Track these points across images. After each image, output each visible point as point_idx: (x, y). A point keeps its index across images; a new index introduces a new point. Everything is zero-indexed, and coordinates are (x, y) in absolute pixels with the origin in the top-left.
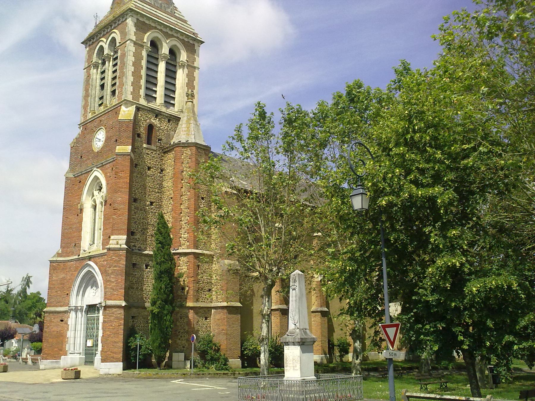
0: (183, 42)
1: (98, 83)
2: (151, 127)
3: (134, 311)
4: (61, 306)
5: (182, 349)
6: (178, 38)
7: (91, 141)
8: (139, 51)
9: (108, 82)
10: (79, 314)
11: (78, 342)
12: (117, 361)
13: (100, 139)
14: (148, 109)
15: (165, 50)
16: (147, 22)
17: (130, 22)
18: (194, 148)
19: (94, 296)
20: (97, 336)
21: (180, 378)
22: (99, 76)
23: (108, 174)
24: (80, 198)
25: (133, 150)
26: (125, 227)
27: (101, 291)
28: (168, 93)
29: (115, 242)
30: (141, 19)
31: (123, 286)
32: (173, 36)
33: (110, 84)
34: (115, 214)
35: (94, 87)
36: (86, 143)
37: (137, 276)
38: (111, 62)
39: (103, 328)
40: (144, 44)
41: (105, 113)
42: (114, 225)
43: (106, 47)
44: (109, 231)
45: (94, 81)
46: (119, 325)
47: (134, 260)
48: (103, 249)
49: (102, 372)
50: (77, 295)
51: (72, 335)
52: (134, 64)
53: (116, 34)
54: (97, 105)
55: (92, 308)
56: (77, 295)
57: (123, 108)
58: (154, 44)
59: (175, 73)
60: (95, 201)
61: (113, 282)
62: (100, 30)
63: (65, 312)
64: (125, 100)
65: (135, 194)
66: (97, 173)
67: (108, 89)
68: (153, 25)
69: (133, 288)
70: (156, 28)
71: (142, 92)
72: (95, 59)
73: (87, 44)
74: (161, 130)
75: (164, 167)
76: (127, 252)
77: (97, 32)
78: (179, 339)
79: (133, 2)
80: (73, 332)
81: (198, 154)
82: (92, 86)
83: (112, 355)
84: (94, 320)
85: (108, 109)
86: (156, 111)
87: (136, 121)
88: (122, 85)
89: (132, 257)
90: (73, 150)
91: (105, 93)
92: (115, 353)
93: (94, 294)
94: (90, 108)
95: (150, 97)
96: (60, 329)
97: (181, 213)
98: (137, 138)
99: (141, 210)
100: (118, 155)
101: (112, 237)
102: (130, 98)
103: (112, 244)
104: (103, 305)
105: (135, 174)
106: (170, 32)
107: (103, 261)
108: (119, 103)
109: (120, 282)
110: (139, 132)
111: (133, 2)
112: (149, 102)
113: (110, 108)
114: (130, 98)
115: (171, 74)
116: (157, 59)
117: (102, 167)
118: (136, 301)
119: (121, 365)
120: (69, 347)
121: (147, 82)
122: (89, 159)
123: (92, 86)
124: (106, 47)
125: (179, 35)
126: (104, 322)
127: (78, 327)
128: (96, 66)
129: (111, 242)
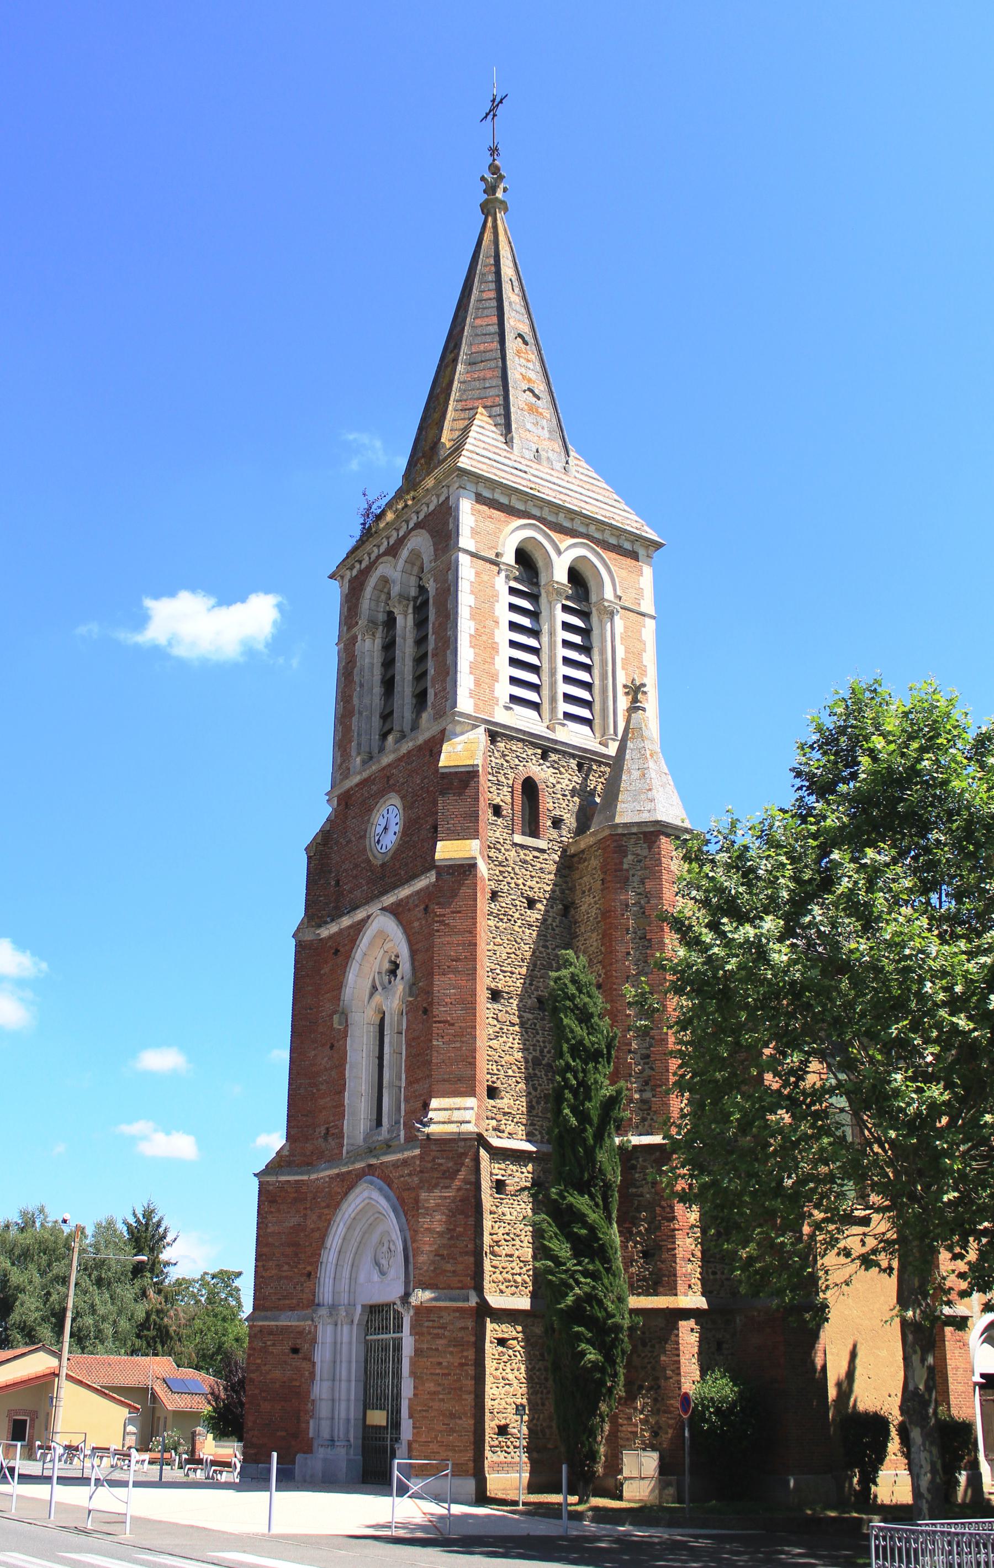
8: (485, 578)
20: (397, 1397)
33: (409, 676)
36: (349, 842)
37: (508, 1217)
38: (410, 618)
39: (413, 1373)
45: (367, 673)
46: (461, 1365)
80: (326, 1385)
82: (362, 686)
94: (359, 745)
101: (435, 1103)
107: (410, 1175)
110: (497, 801)
123: (362, 686)
126: (418, 1352)
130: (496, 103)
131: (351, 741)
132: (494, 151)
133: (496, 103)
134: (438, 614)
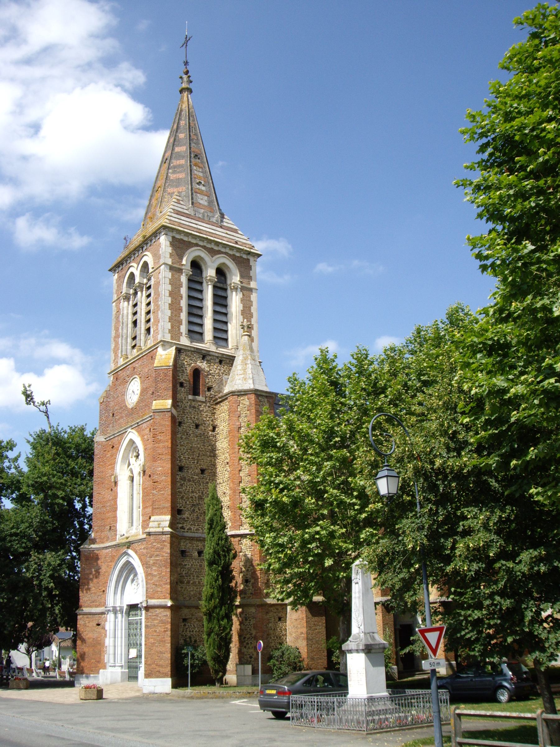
0: (234, 258)
1: (130, 319)
2: (197, 373)
3: (185, 612)
4: (97, 606)
5: (249, 659)
6: (226, 253)
7: (124, 394)
9: (142, 317)
10: (119, 616)
11: (119, 652)
12: (164, 676)
13: (134, 391)
14: (193, 349)
15: (210, 273)
16: (186, 239)
17: (164, 240)
18: (253, 397)
19: (135, 593)
20: (141, 645)
21: (244, 698)
22: (130, 311)
23: (146, 437)
24: (113, 468)
25: (175, 404)
26: (168, 505)
27: (143, 587)
28: (219, 326)
29: (156, 524)
30: (178, 236)
31: (169, 581)
32: (219, 252)
33: (143, 321)
34: (154, 489)
35: (125, 325)
37: (187, 566)
40: (183, 267)
41: (139, 358)
42: (154, 502)
43: (137, 273)
44: (149, 510)
45: (125, 317)
46: (165, 631)
47: (183, 545)
48: (143, 533)
49: (145, 691)
50: (115, 593)
51: (112, 644)
52: (171, 294)
53: (148, 258)
54: (129, 347)
55: (133, 608)
56: (115, 593)
57: (160, 350)
58: (196, 265)
59: (226, 298)
60: (131, 471)
61: (155, 576)
62: (130, 253)
63: (103, 613)
64: (161, 341)
65: (180, 461)
66: (133, 435)
67: (142, 326)
68: (194, 241)
69: (182, 582)
70: (197, 245)
71: (184, 328)
72: (124, 290)
73: (115, 271)
74: (210, 374)
75: (217, 423)
76: (171, 537)
77: (127, 256)
78: (245, 647)
79: (167, 217)
81: (259, 404)
83: (158, 669)
84: (137, 623)
85: (142, 353)
86: (203, 352)
87: (177, 367)
88: (157, 321)
89: (179, 543)
90: (103, 406)
91: (138, 333)
92: (162, 666)
93: (135, 591)
94: (122, 351)
95: (196, 333)
96: (96, 635)
97: (240, 482)
98: (179, 388)
99: (189, 481)
100: (156, 412)
101: (153, 518)
102: (168, 338)
103: (153, 527)
104: (144, 605)
105: (179, 436)
106: (216, 248)
108: (155, 345)
109: (164, 576)
110: (182, 380)
111: (167, 217)
112: (192, 340)
113: (145, 351)
114: (168, 338)
115: (221, 301)
116: (201, 283)
117: (137, 427)
118: (188, 598)
119: (168, 681)
120: (108, 658)
121: (190, 314)
122: (122, 417)
124: (137, 273)
125: (227, 250)
127: (119, 634)
128: (127, 298)
129: (151, 524)
130: (187, 40)
131: (118, 349)
132: (186, 63)
133: (187, 40)
134: (155, 295)
